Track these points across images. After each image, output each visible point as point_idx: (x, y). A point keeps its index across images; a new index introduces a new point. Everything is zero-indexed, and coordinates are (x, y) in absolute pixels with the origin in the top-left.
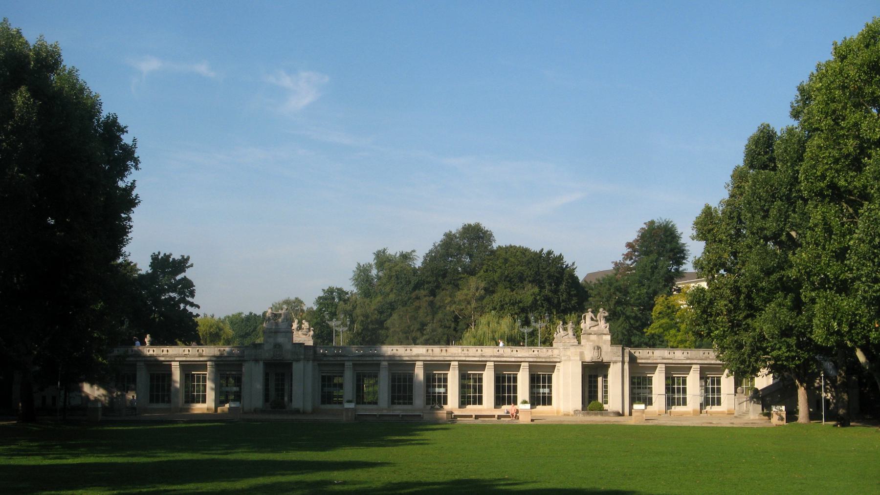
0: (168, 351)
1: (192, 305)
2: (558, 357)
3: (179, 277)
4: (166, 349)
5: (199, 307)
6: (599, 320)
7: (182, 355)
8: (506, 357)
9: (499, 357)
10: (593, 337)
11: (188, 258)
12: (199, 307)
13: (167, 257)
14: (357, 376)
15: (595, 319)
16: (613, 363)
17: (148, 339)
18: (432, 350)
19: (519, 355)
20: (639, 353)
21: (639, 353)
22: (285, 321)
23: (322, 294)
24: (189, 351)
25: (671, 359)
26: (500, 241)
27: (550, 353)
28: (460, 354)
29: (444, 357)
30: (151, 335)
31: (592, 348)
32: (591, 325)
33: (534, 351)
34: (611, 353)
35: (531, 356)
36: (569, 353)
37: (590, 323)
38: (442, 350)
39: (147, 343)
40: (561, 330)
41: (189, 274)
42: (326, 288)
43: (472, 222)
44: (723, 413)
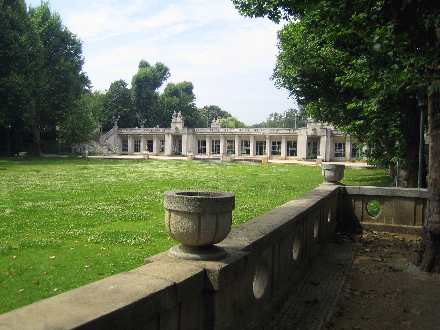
19: (280, 133)
28: (254, 132)
42: (289, 109)
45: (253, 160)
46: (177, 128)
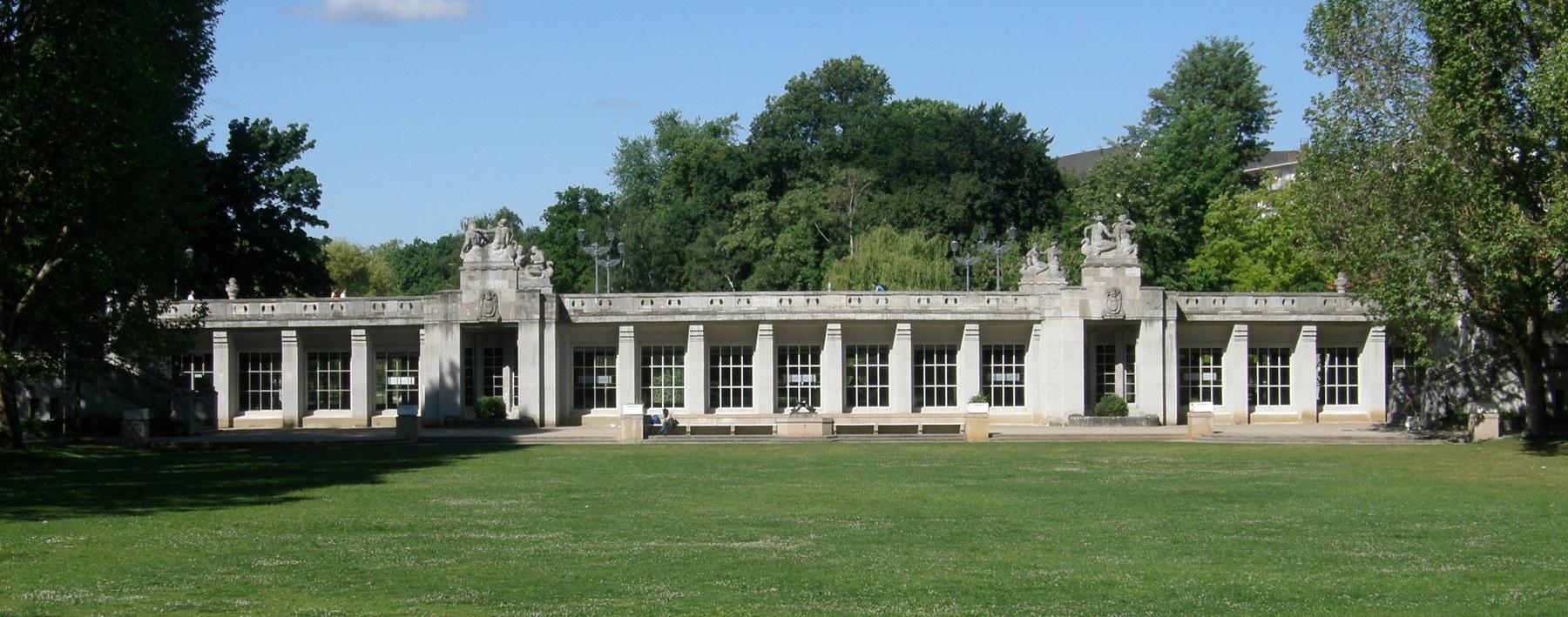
0: (273, 308)
1: (314, 221)
2: (1036, 311)
3: (285, 168)
4: (270, 305)
5: (326, 225)
6: (1118, 238)
7: (301, 315)
8: (936, 312)
9: (920, 313)
10: (1107, 272)
11: (303, 132)
12: (326, 225)
13: (263, 126)
14: (643, 353)
15: (1109, 235)
16: (1146, 321)
17: (231, 287)
18: (790, 301)
19: (959, 309)
20: (1197, 301)
21: (1197, 301)
22: (502, 246)
23: (555, 202)
24: (315, 308)
25: (1260, 313)
26: (904, 89)
27: (1021, 302)
29: (813, 313)
30: (224, 159)
31: (1103, 292)
32: (1102, 249)
33: (988, 302)
34: (1136, 301)
35: (984, 310)
36: (1057, 303)
37: (1100, 244)
38: (808, 301)
39: (230, 294)
40: (1035, 260)
41: (305, 161)
42: (563, 190)
43: (844, 56)
44: (1362, 418)
45: (688, 430)
46: (492, 297)
